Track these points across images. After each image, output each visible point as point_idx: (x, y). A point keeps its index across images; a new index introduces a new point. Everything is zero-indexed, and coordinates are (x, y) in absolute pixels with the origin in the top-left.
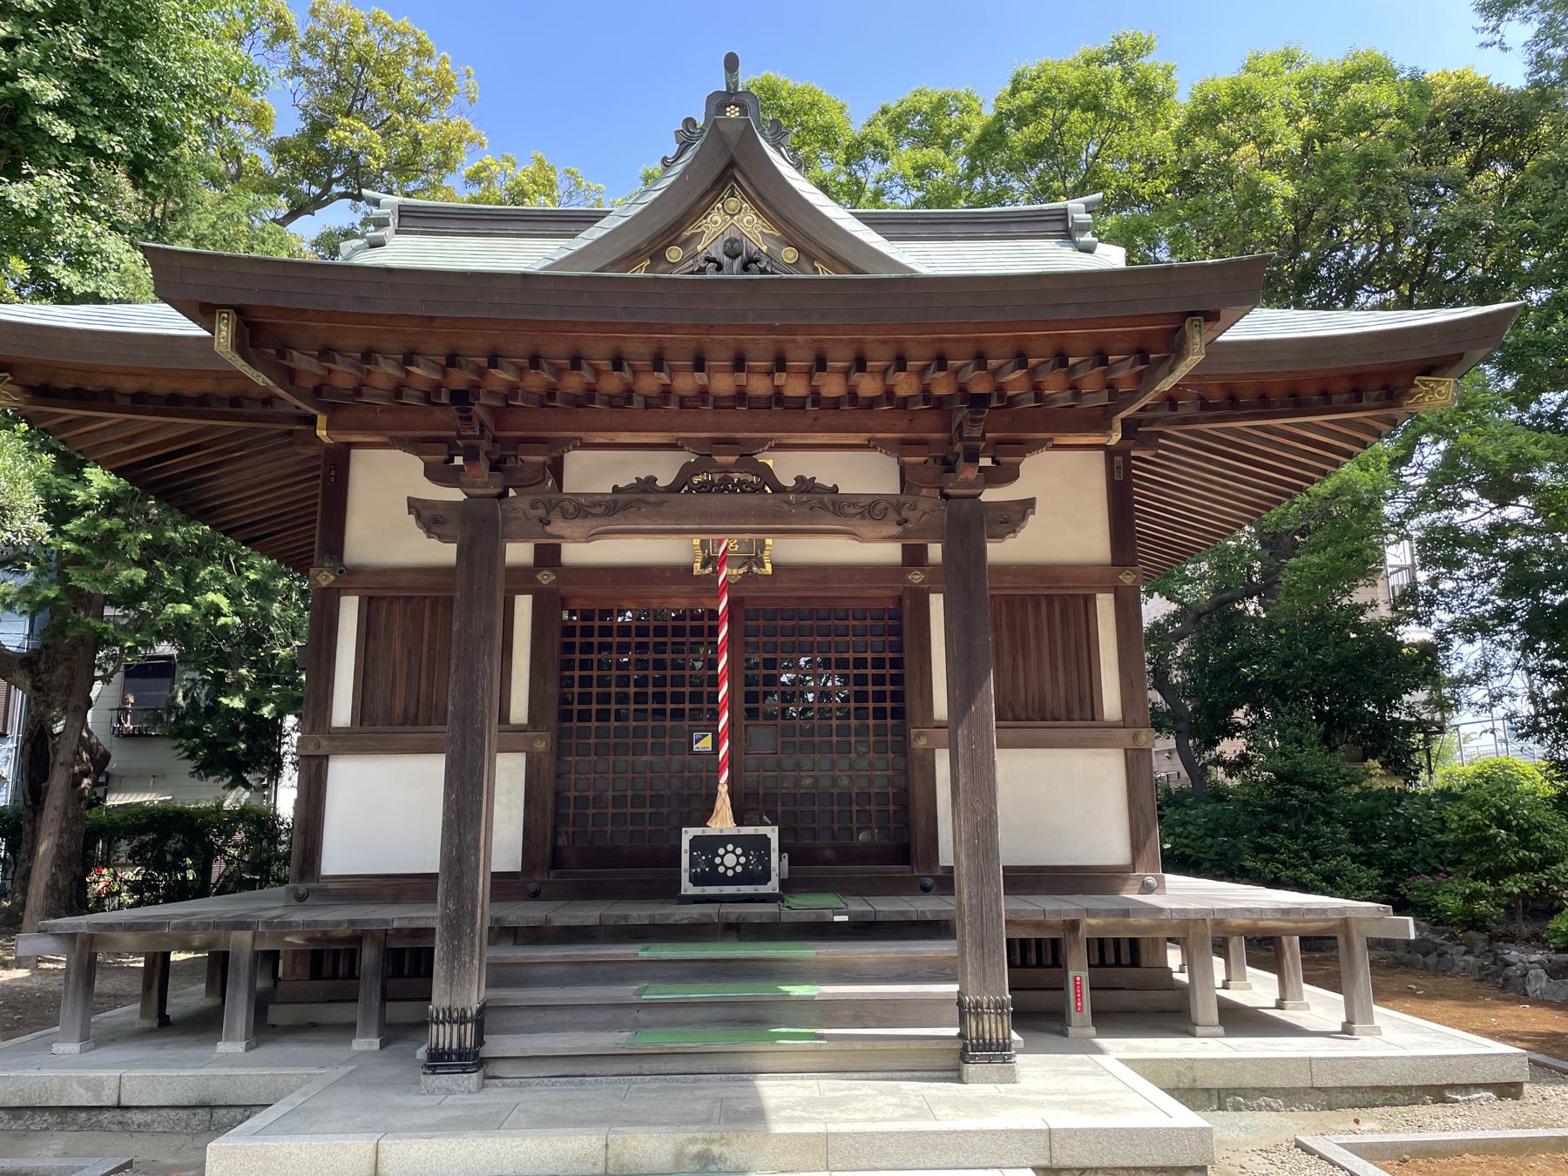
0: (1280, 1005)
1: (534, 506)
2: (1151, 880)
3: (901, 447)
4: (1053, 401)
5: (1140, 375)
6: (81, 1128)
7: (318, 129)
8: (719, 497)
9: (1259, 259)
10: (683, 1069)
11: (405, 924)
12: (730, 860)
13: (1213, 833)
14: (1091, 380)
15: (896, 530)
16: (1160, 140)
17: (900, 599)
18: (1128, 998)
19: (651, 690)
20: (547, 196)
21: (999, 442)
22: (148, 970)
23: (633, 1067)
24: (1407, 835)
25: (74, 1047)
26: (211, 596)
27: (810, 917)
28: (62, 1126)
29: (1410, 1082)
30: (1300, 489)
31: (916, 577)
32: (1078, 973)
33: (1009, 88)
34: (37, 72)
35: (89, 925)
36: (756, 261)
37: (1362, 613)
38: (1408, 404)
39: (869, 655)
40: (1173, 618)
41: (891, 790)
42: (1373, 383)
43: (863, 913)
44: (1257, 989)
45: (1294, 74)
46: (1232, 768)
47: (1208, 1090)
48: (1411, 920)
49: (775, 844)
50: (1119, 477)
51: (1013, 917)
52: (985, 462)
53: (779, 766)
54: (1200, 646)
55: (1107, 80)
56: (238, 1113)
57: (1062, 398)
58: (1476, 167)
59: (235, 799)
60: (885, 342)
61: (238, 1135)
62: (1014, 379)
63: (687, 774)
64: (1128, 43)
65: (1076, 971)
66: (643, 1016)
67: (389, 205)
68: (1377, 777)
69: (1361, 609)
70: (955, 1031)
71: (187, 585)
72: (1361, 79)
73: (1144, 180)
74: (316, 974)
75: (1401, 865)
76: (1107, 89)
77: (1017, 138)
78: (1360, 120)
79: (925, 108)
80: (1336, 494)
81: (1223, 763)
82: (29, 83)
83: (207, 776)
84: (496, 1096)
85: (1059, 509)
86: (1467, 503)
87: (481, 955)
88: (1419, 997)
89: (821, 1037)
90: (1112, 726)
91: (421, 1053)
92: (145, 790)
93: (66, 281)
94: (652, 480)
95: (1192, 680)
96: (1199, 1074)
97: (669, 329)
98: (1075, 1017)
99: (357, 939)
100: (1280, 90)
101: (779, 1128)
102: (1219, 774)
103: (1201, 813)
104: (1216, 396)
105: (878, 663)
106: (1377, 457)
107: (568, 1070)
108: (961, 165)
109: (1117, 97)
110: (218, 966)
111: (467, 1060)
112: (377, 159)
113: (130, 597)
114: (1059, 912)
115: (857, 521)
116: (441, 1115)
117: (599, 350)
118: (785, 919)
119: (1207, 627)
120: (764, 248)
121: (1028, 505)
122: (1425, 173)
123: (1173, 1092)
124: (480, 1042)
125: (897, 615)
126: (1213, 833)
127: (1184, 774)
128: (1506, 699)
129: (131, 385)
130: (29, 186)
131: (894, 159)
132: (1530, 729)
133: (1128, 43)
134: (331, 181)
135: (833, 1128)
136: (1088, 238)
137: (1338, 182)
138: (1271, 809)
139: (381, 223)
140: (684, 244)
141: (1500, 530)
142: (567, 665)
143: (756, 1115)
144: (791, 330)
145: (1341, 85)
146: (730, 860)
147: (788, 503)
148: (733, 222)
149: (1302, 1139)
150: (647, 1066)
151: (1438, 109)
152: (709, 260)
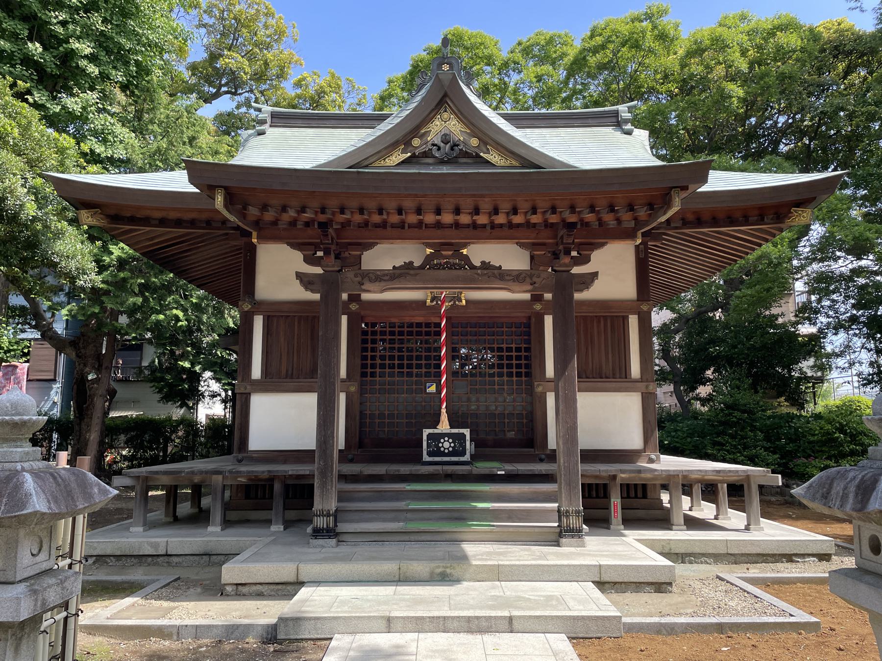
0: (716, 518)
1: (356, 276)
2: (653, 457)
3: (532, 247)
4: (608, 225)
5: (650, 215)
6: (149, 565)
7: (214, 57)
8: (442, 272)
9: (704, 162)
10: (429, 539)
11: (295, 473)
12: (446, 445)
13: (691, 435)
14: (626, 217)
15: (530, 287)
16: (671, 61)
17: (529, 318)
18: (641, 513)
19: (405, 362)
20: (337, 93)
21: (581, 244)
22: (168, 495)
23: (406, 538)
24: (796, 437)
25: (141, 529)
26: (175, 311)
27: (487, 472)
28: (140, 564)
29: (775, 552)
30: (741, 257)
31: (538, 307)
32: (616, 500)
33: (589, 34)
34: (78, 38)
35: (146, 472)
36: (458, 145)
37: (777, 319)
38: (788, 222)
39: (514, 346)
40: (673, 321)
41: (524, 413)
42: (771, 211)
43: (512, 470)
44: (706, 511)
45: (744, 26)
46: (704, 401)
47: (677, 554)
48: (780, 476)
49: (468, 437)
50: (642, 256)
51: (585, 473)
52: (574, 253)
53: (469, 400)
54: (689, 335)
55: (643, 32)
56: (222, 558)
57: (612, 224)
58: (847, 72)
59: (178, 413)
60: (527, 201)
61: (235, 562)
62: (589, 217)
63: (423, 404)
64: (655, 9)
65: (615, 498)
66: (409, 515)
67: (266, 112)
68: (784, 407)
69: (776, 317)
70: (556, 524)
71: (161, 305)
72: (782, 30)
73: (662, 84)
74: (247, 497)
75: (790, 452)
76: (643, 37)
77: (592, 60)
78: (781, 54)
79: (543, 43)
80: (760, 258)
81: (700, 399)
82: (75, 45)
83: (167, 402)
84: (344, 549)
85: (611, 272)
86: (839, 258)
87: (335, 487)
88: (793, 519)
89: (493, 526)
90: (636, 381)
91: (309, 530)
92: (129, 409)
93: (98, 151)
94: (411, 263)
95: (684, 354)
96: (673, 547)
97: (424, 196)
98: (614, 520)
99: (271, 480)
100: (736, 37)
101: (474, 563)
102: (697, 405)
103: (684, 426)
104: (690, 217)
105: (518, 350)
106: (782, 239)
107: (376, 538)
108: (562, 74)
109: (649, 41)
110: (198, 492)
111: (329, 533)
112: (246, 74)
113: (131, 312)
114: (607, 471)
115: (510, 283)
116: (323, 556)
117: (391, 205)
118: (474, 472)
119: (692, 326)
120: (462, 139)
121: (595, 275)
122: (817, 80)
123: (661, 554)
124: (336, 526)
125: (528, 326)
126: (691, 435)
127: (678, 405)
128: (857, 365)
129: (158, 215)
130: (76, 99)
131: (525, 72)
132: (867, 382)
133: (655, 9)
134: (221, 86)
135: (501, 563)
136: (629, 127)
137: (768, 88)
138: (722, 423)
139: (263, 122)
140: (422, 137)
141: (857, 272)
142: (365, 350)
143: (464, 558)
144: (482, 196)
145: (772, 33)
146: (446, 445)
147: (478, 274)
148: (446, 126)
149: (720, 575)
150: (412, 538)
151: (826, 43)
152: (434, 145)
